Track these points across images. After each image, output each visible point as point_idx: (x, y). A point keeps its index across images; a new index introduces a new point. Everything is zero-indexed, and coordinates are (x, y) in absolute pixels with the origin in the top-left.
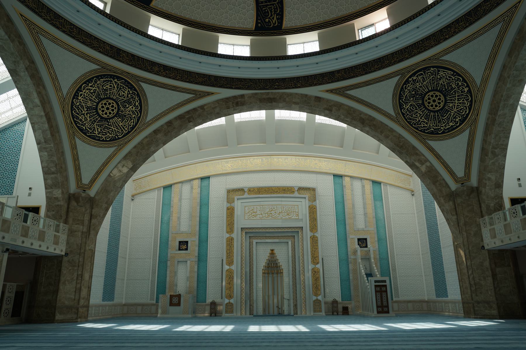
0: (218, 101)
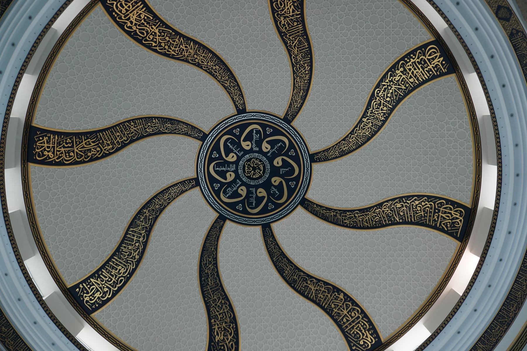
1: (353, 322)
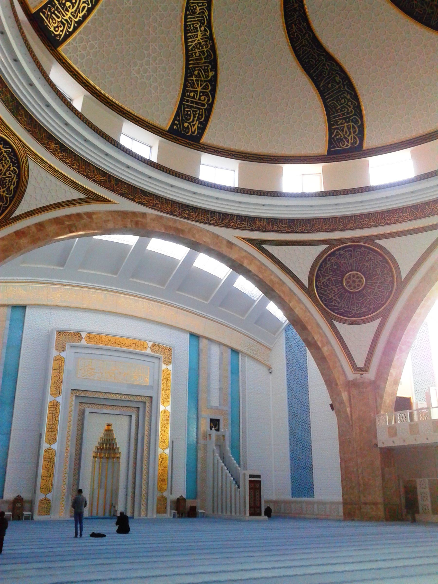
0: (112, 213)
1: (197, 103)
